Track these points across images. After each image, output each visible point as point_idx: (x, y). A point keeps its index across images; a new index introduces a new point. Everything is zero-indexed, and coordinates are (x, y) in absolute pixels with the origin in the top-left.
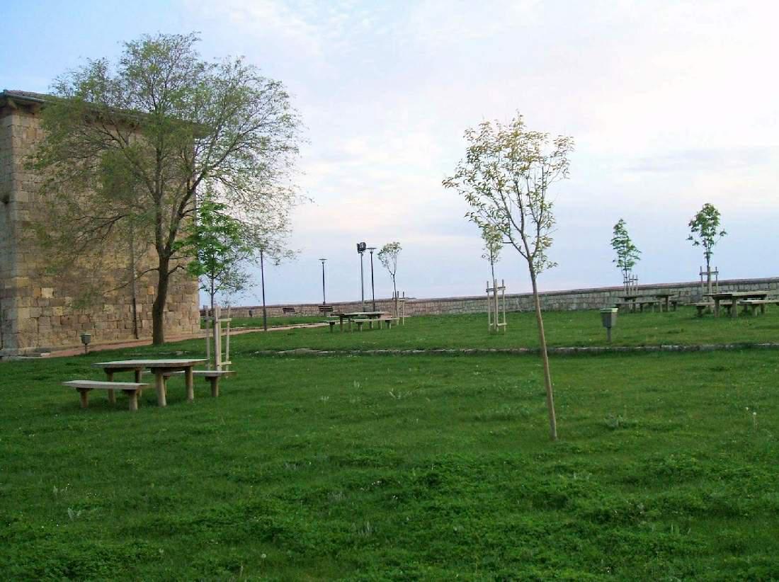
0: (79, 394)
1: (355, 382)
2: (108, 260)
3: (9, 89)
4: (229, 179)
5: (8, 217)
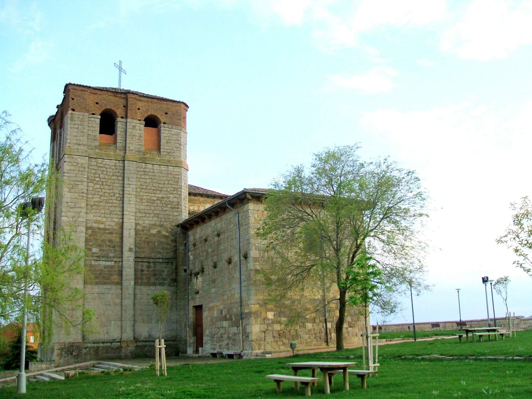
0: (276, 384)
1: (462, 381)
2: (307, 293)
3: (247, 188)
4: (384, 238)
5: (247, 267)
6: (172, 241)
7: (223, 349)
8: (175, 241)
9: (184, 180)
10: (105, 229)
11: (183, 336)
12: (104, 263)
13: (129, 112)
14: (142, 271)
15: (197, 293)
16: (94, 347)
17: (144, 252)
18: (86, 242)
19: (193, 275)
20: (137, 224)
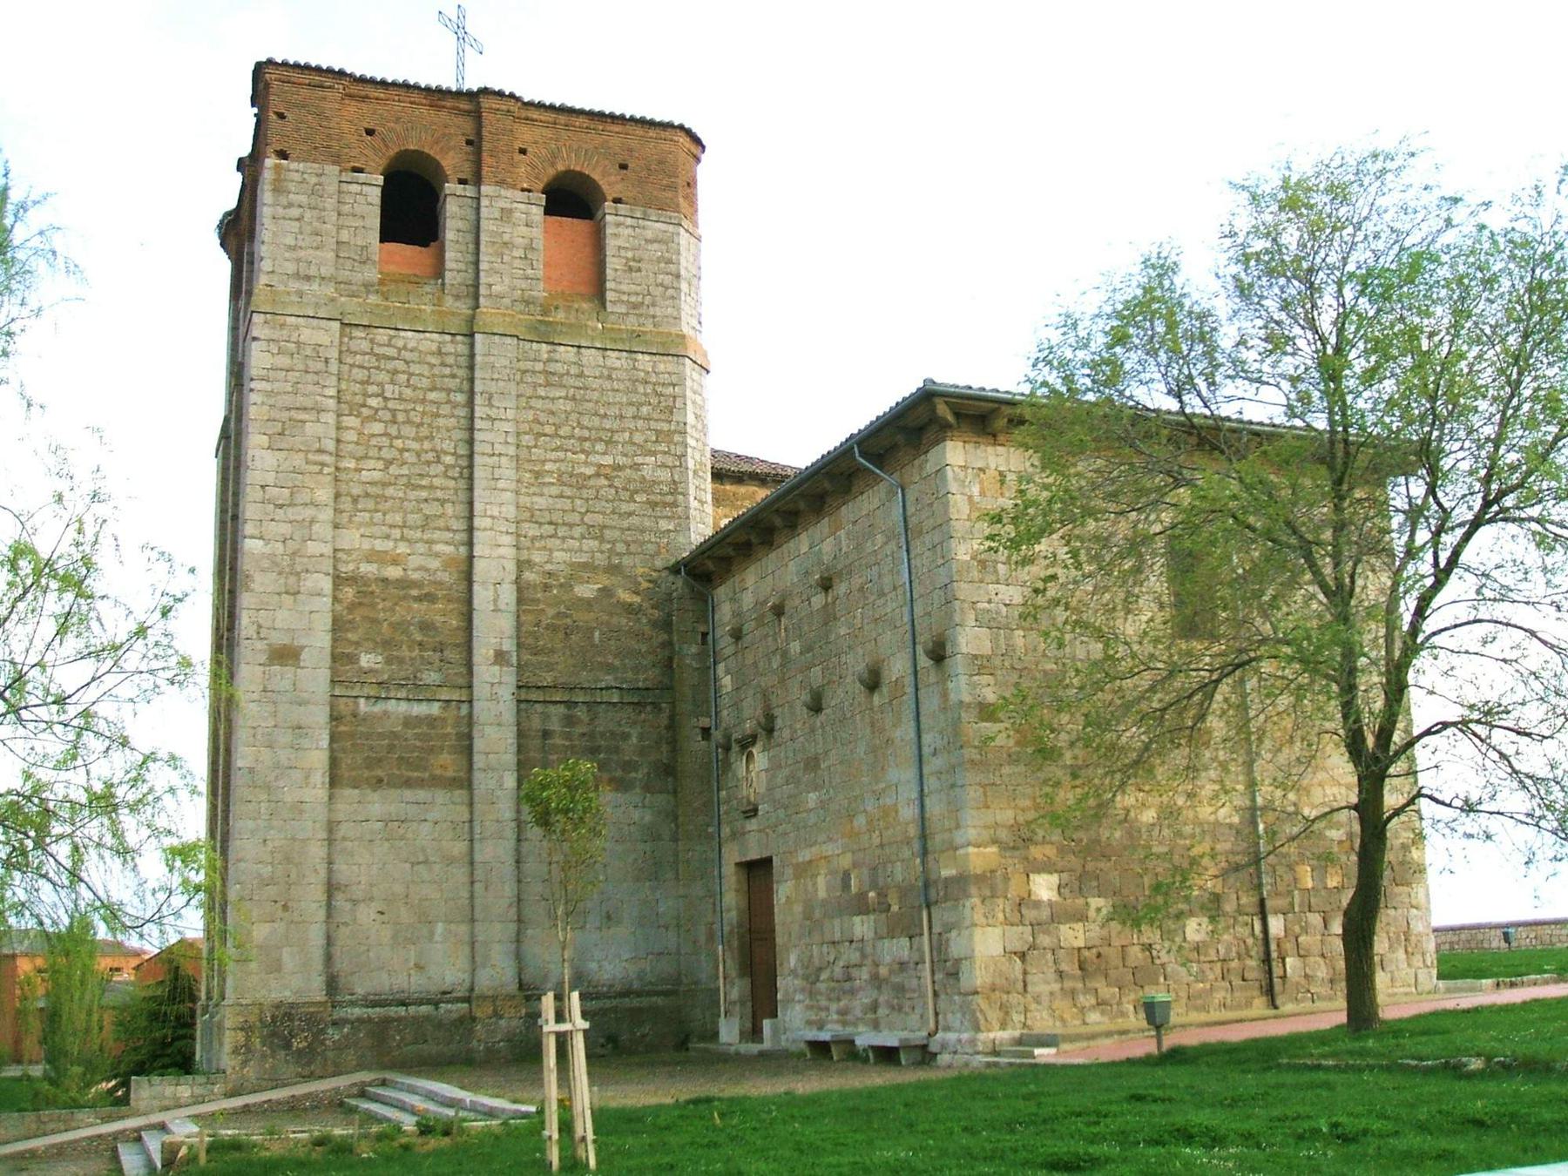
5: (945, 695)
6: (654, 624)
7: (855, 1024)
8: (666, 625)
9: (694, 402)
10: (404, 584)
11: (703, 976)
12: (403, 707)
13: (487, 159)
14: (546, 734)
15: (752, 812)
16: (370, 1020)
17: (550, 667)
18: (333, 630)
19: (735, 748)
20: (522, 565)
